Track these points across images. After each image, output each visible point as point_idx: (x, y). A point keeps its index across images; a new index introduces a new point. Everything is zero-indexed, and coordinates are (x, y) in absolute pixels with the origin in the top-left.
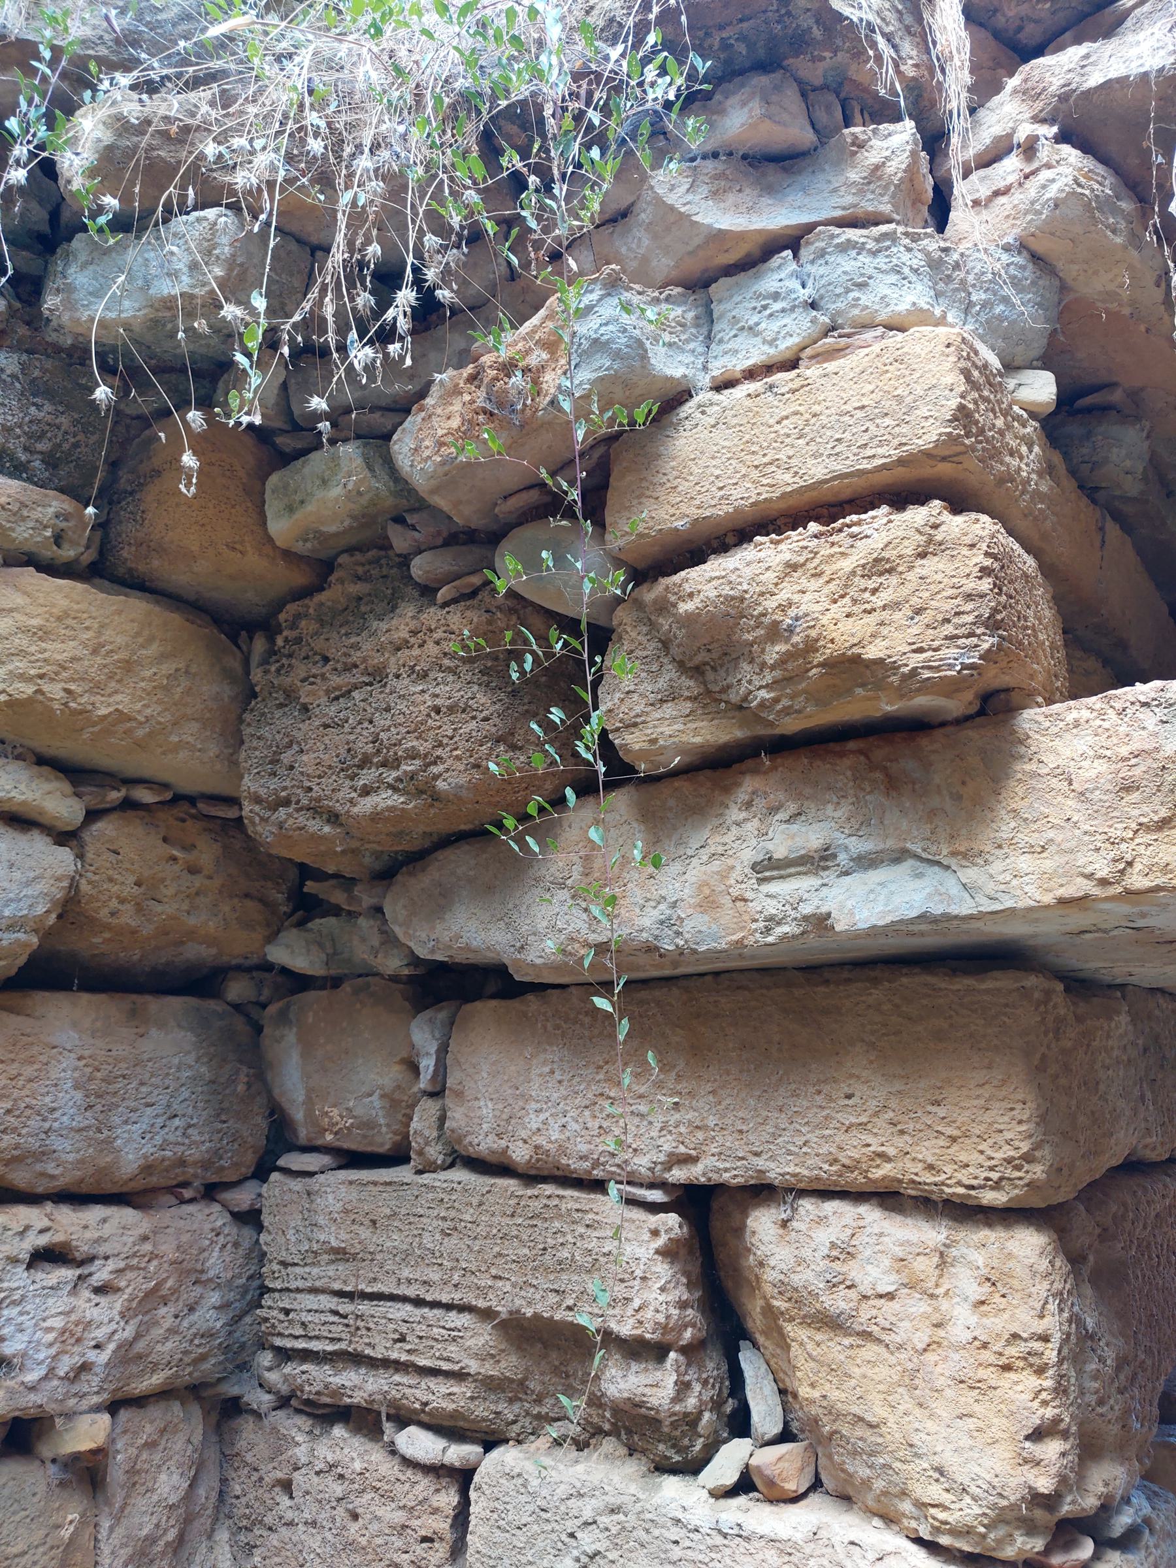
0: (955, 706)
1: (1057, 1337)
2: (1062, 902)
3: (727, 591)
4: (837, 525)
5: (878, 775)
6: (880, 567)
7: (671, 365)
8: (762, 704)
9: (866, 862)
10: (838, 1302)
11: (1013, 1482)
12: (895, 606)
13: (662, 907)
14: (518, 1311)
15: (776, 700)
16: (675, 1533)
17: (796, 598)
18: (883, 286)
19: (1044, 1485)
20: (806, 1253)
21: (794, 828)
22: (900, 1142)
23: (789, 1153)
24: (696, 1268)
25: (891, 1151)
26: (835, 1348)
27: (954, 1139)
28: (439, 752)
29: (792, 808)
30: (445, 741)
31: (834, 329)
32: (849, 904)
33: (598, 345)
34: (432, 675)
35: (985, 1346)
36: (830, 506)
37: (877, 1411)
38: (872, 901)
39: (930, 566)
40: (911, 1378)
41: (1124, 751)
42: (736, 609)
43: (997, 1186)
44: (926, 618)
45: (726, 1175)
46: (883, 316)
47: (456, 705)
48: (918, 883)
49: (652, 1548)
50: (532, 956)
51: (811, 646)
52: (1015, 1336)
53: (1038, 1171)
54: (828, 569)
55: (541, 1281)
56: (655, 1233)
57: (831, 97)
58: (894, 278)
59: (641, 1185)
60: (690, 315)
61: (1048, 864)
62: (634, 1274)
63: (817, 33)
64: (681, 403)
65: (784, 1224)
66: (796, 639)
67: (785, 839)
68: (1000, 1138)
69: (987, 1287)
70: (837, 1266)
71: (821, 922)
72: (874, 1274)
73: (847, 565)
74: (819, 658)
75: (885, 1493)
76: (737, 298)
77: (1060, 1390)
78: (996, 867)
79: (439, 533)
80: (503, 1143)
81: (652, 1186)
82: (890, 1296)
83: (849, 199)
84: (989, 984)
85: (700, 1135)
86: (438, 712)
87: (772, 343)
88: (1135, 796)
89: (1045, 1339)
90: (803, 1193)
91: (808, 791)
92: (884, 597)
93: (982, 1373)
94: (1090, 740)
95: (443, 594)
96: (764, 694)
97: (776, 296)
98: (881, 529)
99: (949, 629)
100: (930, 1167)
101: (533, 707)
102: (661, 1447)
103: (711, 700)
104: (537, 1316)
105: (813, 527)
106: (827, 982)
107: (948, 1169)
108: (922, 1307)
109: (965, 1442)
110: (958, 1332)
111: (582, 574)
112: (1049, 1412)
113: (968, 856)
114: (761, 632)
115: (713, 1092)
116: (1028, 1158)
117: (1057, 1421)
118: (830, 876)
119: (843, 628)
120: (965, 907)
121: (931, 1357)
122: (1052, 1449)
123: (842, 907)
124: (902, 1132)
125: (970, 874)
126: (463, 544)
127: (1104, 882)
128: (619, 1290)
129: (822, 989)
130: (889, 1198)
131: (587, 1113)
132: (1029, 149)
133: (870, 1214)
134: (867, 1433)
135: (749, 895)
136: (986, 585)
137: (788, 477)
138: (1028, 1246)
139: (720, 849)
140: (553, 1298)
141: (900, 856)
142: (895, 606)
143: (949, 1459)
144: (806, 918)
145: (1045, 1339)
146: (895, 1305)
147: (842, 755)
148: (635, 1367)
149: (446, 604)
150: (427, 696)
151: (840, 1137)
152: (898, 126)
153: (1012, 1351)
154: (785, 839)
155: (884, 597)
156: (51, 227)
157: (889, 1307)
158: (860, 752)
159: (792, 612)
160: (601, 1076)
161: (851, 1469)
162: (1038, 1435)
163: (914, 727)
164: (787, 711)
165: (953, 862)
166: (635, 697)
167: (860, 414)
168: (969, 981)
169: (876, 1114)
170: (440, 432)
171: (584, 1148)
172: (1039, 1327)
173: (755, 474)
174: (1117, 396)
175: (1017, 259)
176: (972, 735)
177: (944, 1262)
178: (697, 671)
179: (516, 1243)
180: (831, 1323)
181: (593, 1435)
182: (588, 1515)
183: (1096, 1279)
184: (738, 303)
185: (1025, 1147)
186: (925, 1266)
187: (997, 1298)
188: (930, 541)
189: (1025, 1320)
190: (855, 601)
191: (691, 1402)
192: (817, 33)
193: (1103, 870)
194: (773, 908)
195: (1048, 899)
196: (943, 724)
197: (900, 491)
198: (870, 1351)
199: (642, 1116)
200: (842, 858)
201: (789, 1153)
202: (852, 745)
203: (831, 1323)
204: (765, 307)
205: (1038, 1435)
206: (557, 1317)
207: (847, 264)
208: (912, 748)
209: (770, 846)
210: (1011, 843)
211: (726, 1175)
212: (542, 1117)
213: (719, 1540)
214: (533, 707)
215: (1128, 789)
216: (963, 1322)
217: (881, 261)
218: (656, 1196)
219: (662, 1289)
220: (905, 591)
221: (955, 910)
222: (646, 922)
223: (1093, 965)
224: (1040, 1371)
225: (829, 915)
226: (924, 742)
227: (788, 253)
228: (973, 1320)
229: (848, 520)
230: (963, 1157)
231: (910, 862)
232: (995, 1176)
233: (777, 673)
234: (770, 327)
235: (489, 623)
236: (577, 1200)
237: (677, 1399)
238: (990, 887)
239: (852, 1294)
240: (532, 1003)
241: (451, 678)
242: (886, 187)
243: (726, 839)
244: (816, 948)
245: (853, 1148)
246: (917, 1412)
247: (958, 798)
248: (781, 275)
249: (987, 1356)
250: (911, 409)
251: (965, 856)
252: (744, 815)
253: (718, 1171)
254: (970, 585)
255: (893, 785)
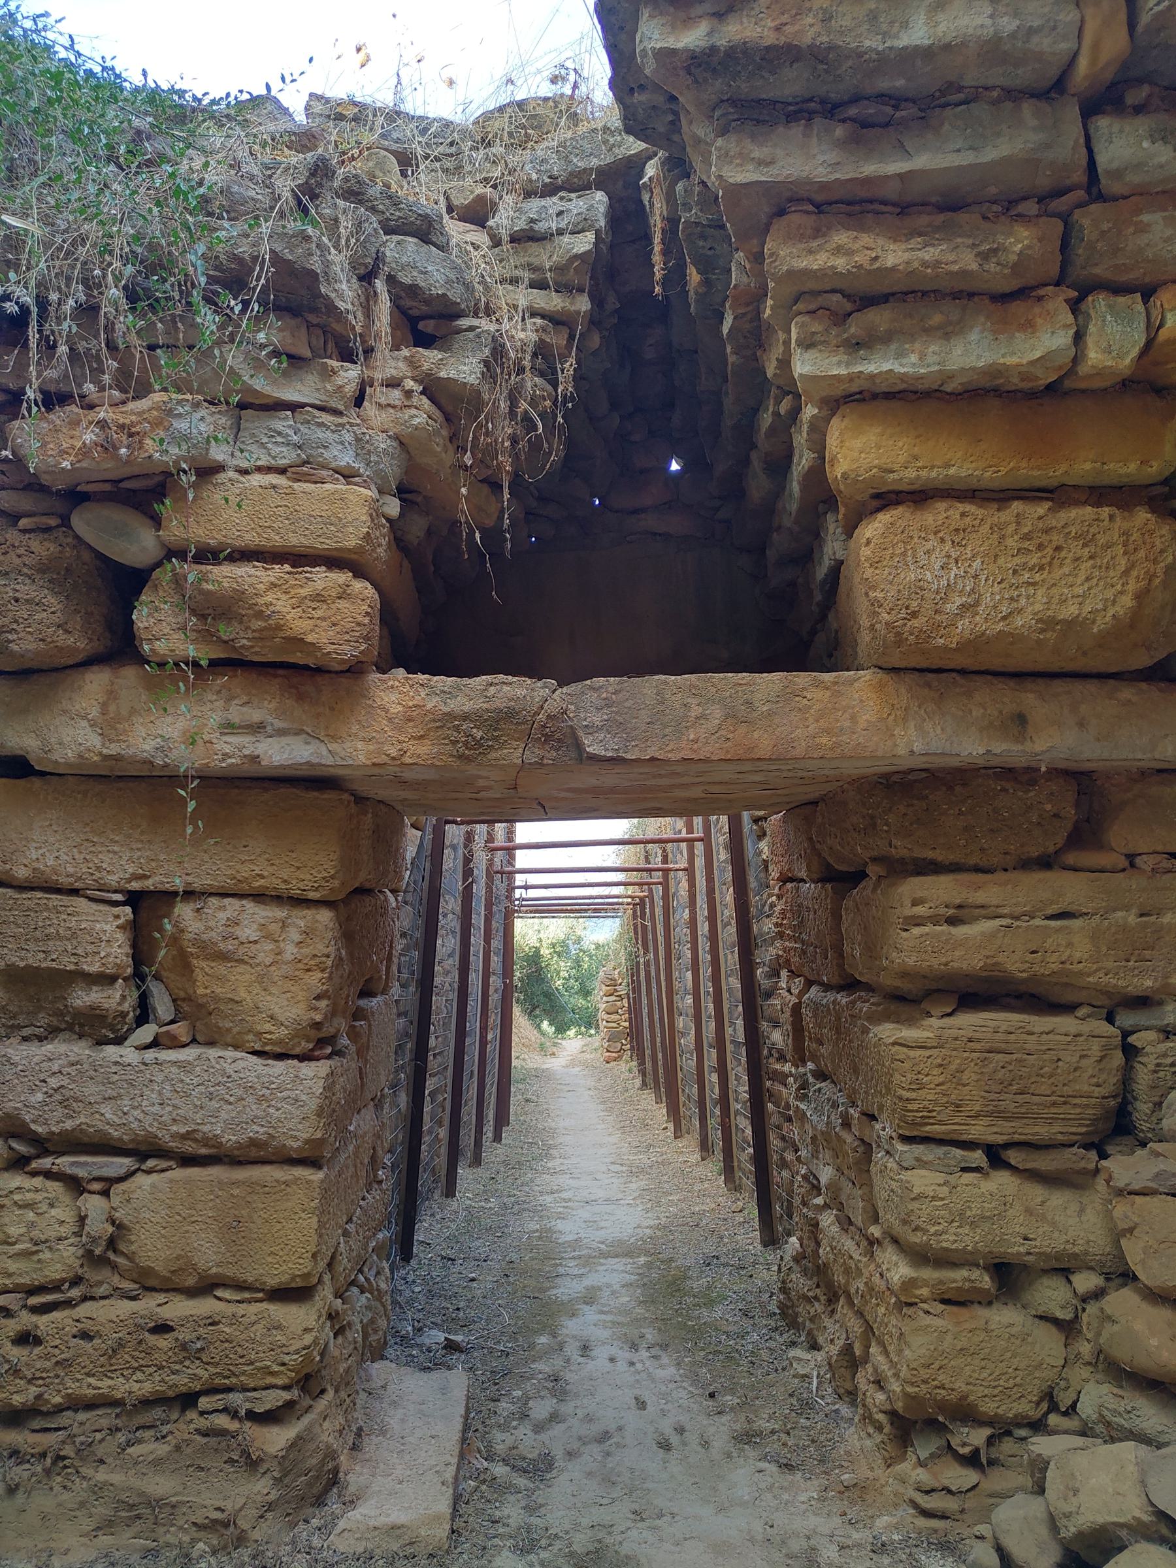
0: (338, 668)
1: (333, 956)
2: (374, 764)
3: (235, 586)
4: (300, 569)
5: (293, 690)
6: (318, 597)
7: (218, 453)
8: (243, 647)
9: (281, 733)
10: (230, 946)
11: (305, 1018)
12: (324, 619)
13: (159, 740)
14: (13, 964)
15: (252, 647)
16: (114, 1069)
17: (274, 601)
18: (335, 450)
19: (318, 1018)
20: (212, 924)
21: (245, 709)
22: (270, 869)
23: (208, 874)
24: (131, 937)
25: (266, 874)
26: (221, 969)
27: (298, 868)
28: (15, 626)
29: (245, 698)
30: (21, 620)
31: (308, 463)
32: (270, 752)
33: (186, 438)
34: (13, 576)
35: (300, 961)
36: (299, 559)
37: (242, 994)
38: (282, 752)
39: (342, 604)
40: (260, 979)
41: (410, 704)
42: (239, 596)
43: (317, 890)
44: (338, 629)
45: (167, 885)
46: (333, 465)
47: (33, 599)
48: (308, 747)
49: (99, 1079)
50: (56, 756)
51: (279, 627)
52: (315, 956)
53: (336, 883)
54: (293, 592)
55: (31, 946)
56: (117, 917)
57: (320, 332)
58: (340, 447)
59: (108, 891)
60: (229, 423)
61: (371, 748)
62: (105, 936)
63: (323, 310)
64: (218, 472)
65: (198, 910)
66: (271, 622)
67: (237, 713)
68: (321, 868)
69: (304, 936)
70: (229, 929)
71: (255, 759)
72: (248, 932)
73: (303, 592)
74: (281, 634)
75: (239, 1033)
76: (256, 424)
77: (330, 978)
78: (347, 745)
79: (22, 481)
80: (8, 867)
81: (115, 892)
82: (256, 942)
83: (324, 398)
84: (325, 796)
85: (154, 864)
86: (17, 601)
87: (274, 458)
88: (412, 724)
89: (328, 956)
90: (211, 894)
91: (254, 692)
92: (318, 613)
93: (297, 973)
94: (397, 696)
95: (23, 523)
96: (245, 641)
97: (280, 434)
98: (322, 578)
99: (347, 637)
100: (285, 881)
101: (78, 607)
102: (103, 1031)
103: (206, 636)
104: (27, 967)
105: (287, 567)
106: (237, 787)
107: (294, 882)
108: (269, 946)
109: (286, 1003)
110: (288, 956)
111: (137, 544)
112: (325, 987)
113: (334, 738)
114: (251, 612)
115: (165, 842)
116: (332, 877)
117: (327, 991)
118: (261, 737)
119: (298, 624)
120: (329, 761)
121: (272, 968)
122: (323, 1004)
123: (266, 752)
124: (273, 864)
125: (334, 746)
126: (36, 491)
127: (394, 759)
128: (90, 948)
129: (236, 791)
130: (259, 897)
131: (75, 850)
132: (408, 394)
133: (248, 905)
134: (235, 1006)
135: (214, 741)
136: (366, 620)
137: (277, 538)
138: (325, 916)
139: (200, 714)
140: (41, 956)
141: (299, 732)
142: (324, 619)
143: (277, 1011)
144: (245, 756)
145: (328, 956)
146: (258, 946)
147: (275, 676)
148: (95, 988)
149: (24, 531)
150: (8, 589)
151: (239, 866)
152: (353, 366)
153: (312, 962)
154: (237, 713)
155: (318, 613)
156: (13, 402)
157: (253, 947)
158: (284, 676)
159: (272, 608)
160: (88, 829)
161: (221, 1025)
162: (318, 998)
163: (319, 671)
164: (256, 653)
165: (326, 740)
166: (164, 624)
167: (319, 519)
168: (316, 794)
169: (260, 856)
170: (65, 445)
171: (71, 870)
172: (326, 951)
173: (259, 530)
174: (419, 499)
175: (394, 444)
176: (344, 681)
177: (284, 926)
178: (203, 617)
179: (12, 926)
180: (223, 957)
181: (51, 1033)
182: (55, 1068)
183: (818, 535)
184: (255, 424)
185: (332, 872)
186: (274, 927)
187: (308, 940)
188: (344, 592)
189: (320, 948)
190: (304, 612)
191: (126, 1005)
192: (323, 310)
193: (394, 752)
194: (228, 749)
195: (369, 762)
196: (329, 672)
197: (333, 561)
198: (242, 968)
199: (115, 853)
200: (269, 728)
201: (208, 874)
202: (280, 672)
203: (223, 957)
204: (273, 437)
205: (318, 998)
206: (43, 965)
207: (320, 434)
208: (301, 677)
209: (230, 717)
210: (356, 735)
211: (167, 885)
212: (40, 852)
213: (143, 1067)
214: (78, 607)
215: (410, 720)
216: (290, 951)
217: (336, 436)
218: (118, 897)
219: (119, 946)
220: (329, 613)
221: (323, 762)
222: (147, 747)
223: (365, 790)
224: (323, 971)
225: (258, 757)
226: (319, 679)
227: (289, 413)
228: (296, 950)
229: (306, 569)
230: (302, 877)
231: (304, 736)
232: (316, 885)
233: (257, 635)
234: (276, 450)
235: (60, 552)
236: (60, 900)
237: (119, 1004)
238: (343, 754)
239: (236, 942)
240: (37, 782)
241: (27, 581)
242: (343, 398)
243: (202, 709)
244: (250, 770)
245: (245, 872)
246: (263, 993)
247: (332, 709)
248: (283, 423)
249: (300, 966)
250: (344, 526)
251: (332, 737)
252: (215, 697)
253: (162, 883)
254: (360, 619)
255: (301, 697)
